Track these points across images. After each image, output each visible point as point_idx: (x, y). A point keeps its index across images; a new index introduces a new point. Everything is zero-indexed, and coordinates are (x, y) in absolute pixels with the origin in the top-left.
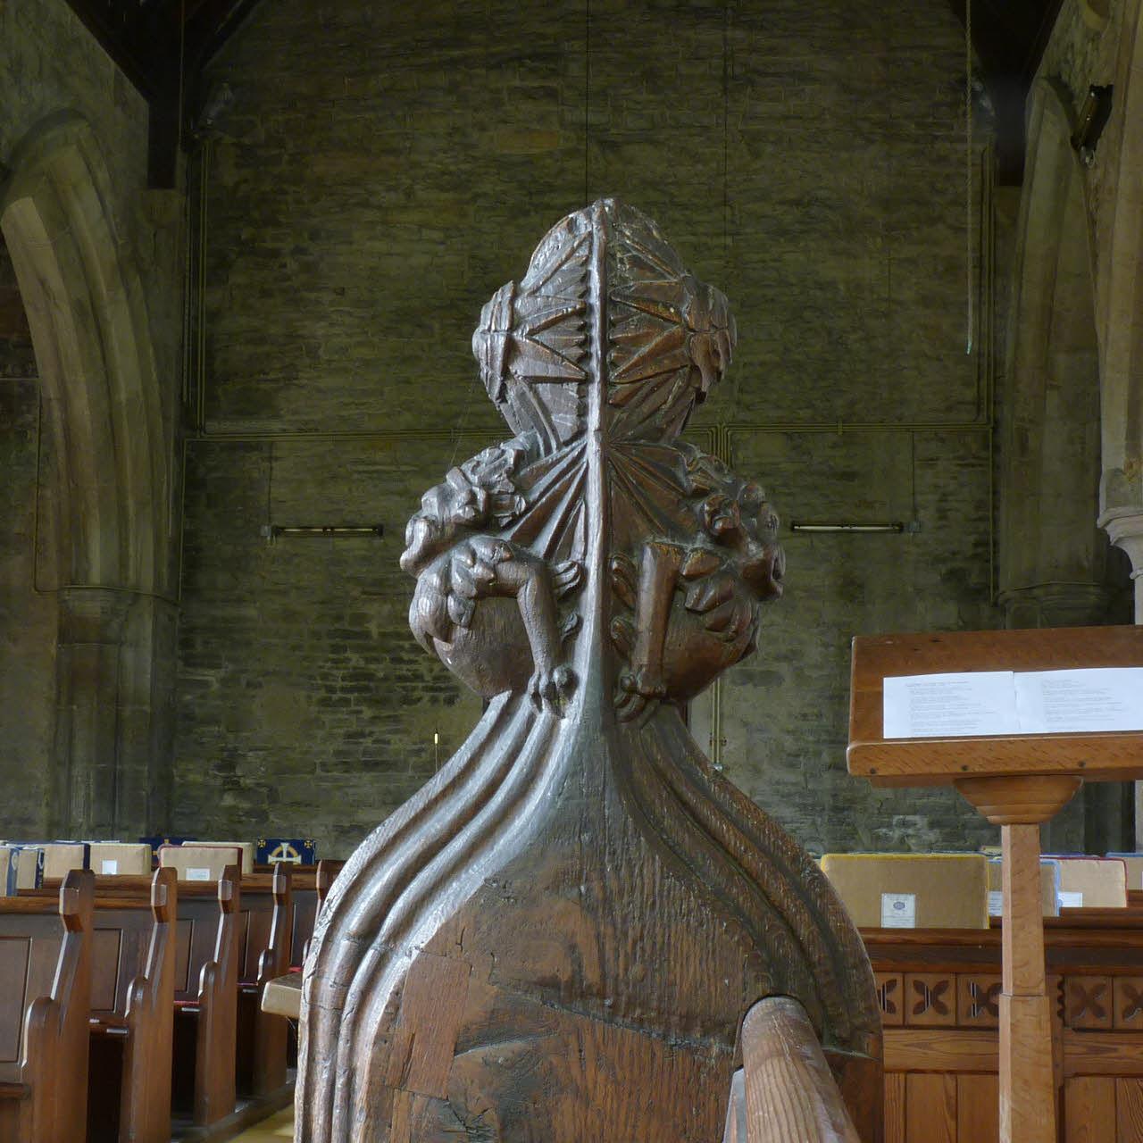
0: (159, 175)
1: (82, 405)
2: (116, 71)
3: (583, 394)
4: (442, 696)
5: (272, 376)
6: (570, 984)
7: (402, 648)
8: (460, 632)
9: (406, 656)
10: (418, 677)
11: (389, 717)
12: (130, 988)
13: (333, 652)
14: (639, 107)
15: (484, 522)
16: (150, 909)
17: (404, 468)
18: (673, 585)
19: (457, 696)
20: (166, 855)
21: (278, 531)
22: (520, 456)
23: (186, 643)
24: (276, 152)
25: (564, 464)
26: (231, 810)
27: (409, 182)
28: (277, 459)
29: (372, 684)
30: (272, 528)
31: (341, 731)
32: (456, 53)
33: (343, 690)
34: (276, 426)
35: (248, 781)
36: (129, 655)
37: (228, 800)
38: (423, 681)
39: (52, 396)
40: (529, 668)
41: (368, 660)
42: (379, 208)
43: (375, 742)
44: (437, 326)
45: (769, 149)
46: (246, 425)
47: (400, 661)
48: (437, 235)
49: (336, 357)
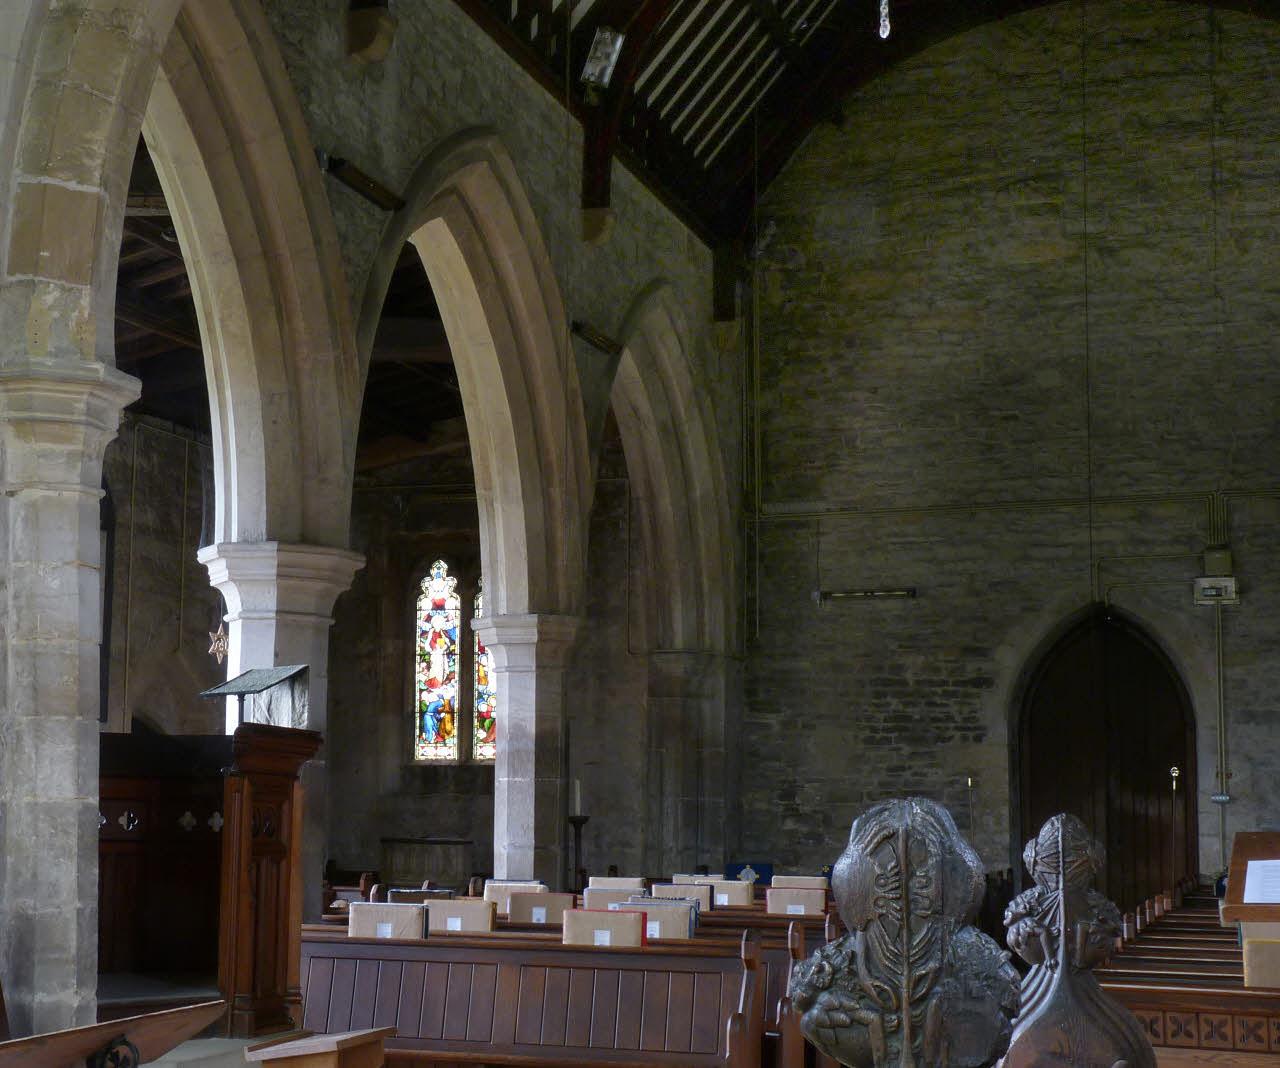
0: (723, 311)
1: (666, 503)
2: (690, 241)
3: (1057, 877)
4: (971, 734)
5: (817, 464)
6: (1060, 1054)
7: (935, 694)
8: (1023, 947)
9: (938, 700)
10: (950, 718)
11: (927, 753)
12: (779, 1004)
13: (876, 698)
14: (1133, 215)
15: (1030, 913)
16: (787, 949)
17: (932, 539)
18: (1086, 935)
19: (984, 735)
20: (771, 894)
21: (825, 596)
22: (1040, 895)
23: (751, 692)
24: (816, 274)
25: (1051, 899)
26: (791, 833)
27: (929, 293)
28: (823, 534)
29: (910, 725)
30: (821, 593)
31: (885, 766)
32: (967, 180)
33: (885, 730)
34: (821, 506)
35: (805, 808)
36: (706, 706)
37: (790, 825)
38: (955, 722)
39: (641, 495)
40: (1044, 959)
41: (906, 704)
42: (906, 317)
43: (915, 774)
44: (957, 417)
45: (1257, 243)
46: (796, 507)
47: (931, 704)
48: (954, 338)
49: (871, 446)
